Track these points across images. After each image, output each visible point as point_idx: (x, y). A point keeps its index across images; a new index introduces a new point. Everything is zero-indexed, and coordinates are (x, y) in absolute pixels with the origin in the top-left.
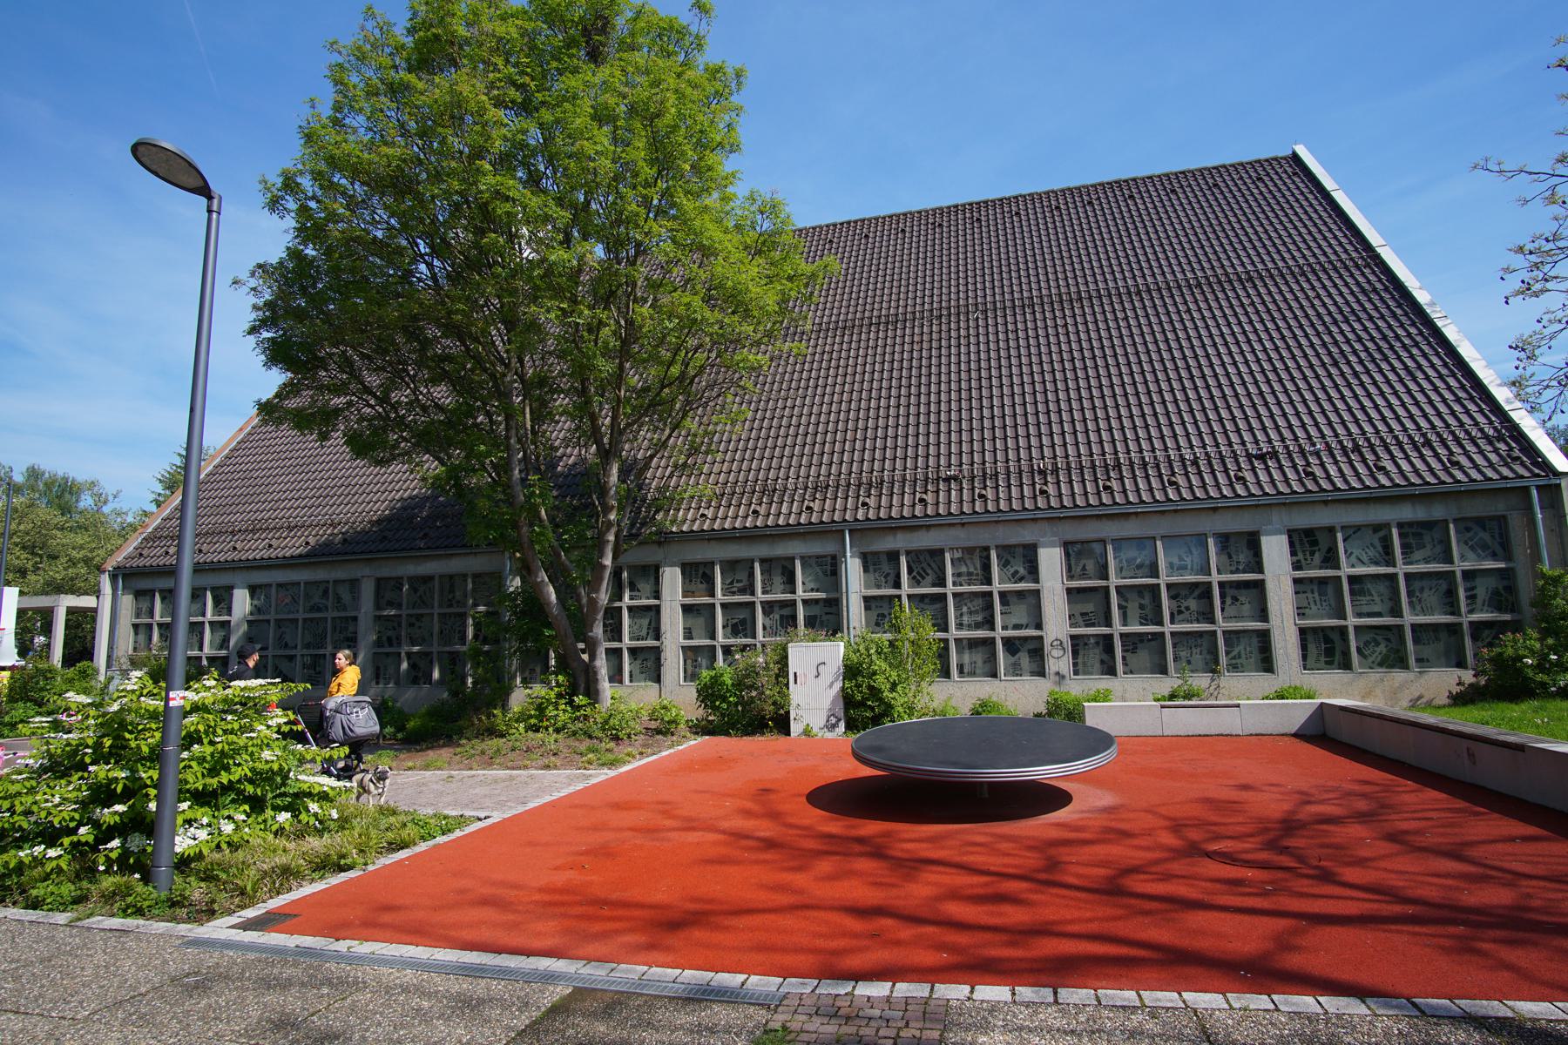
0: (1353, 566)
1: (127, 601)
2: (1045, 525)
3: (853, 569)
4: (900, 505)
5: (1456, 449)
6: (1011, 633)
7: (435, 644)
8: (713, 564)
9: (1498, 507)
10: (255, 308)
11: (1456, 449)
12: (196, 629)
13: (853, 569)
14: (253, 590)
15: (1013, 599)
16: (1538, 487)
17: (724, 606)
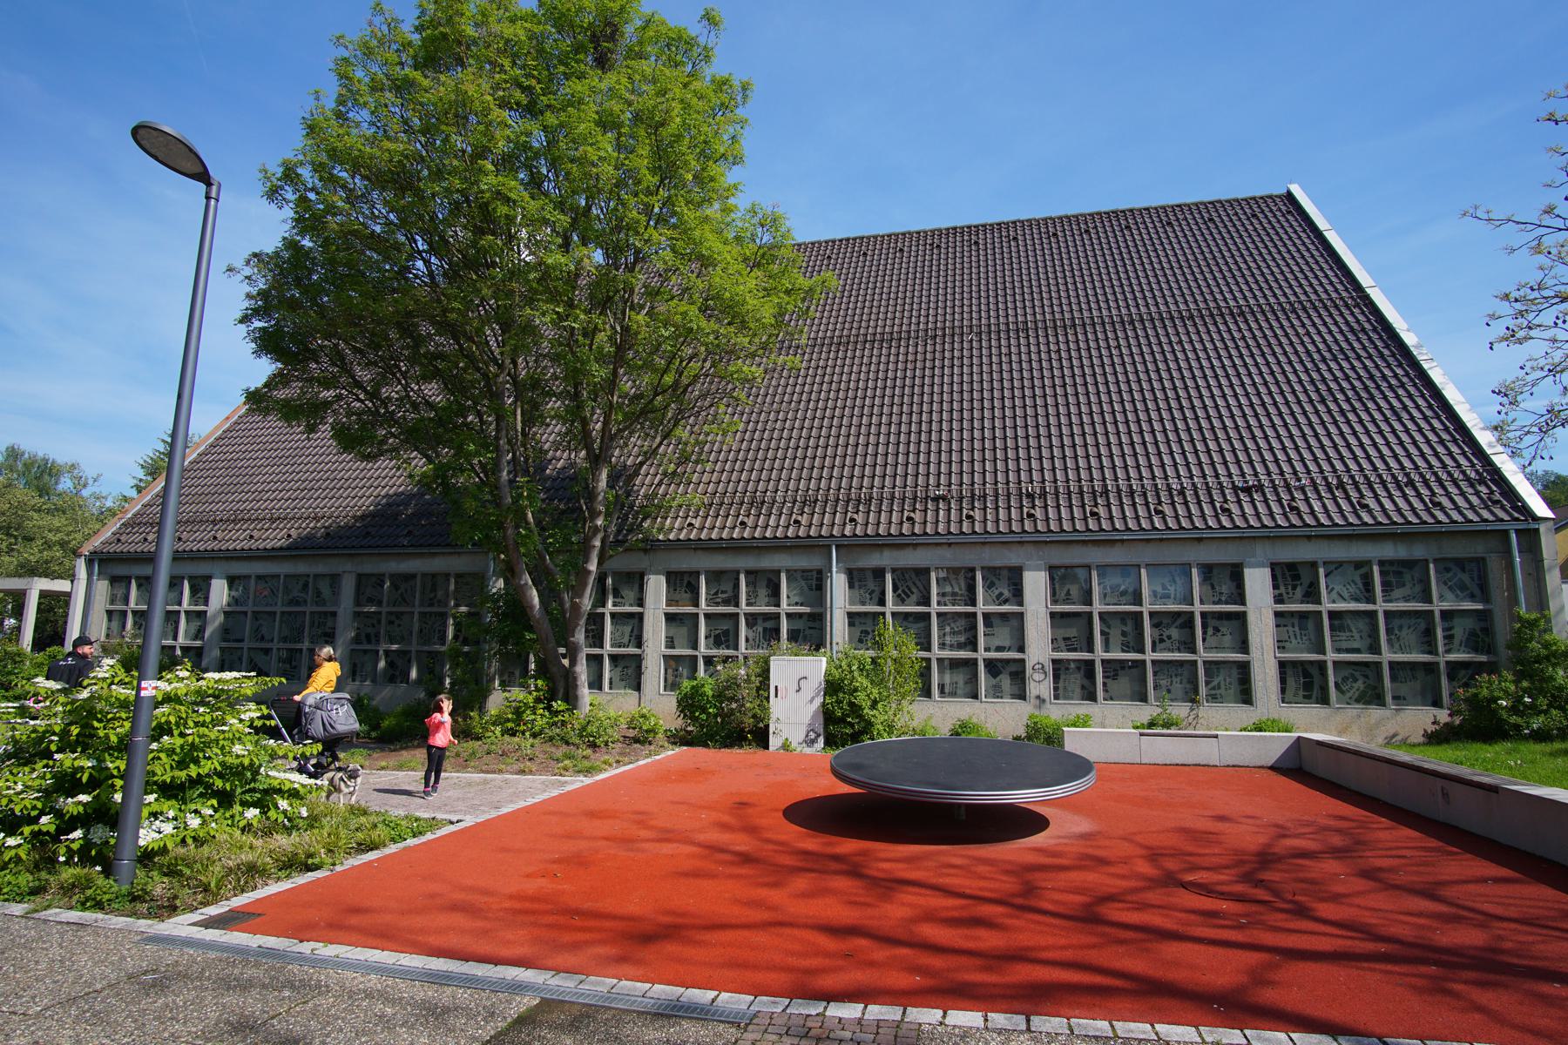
0: (1334, 602)
1: (102, 587)
2: (1030, 549)
3: (838, 584)
4: (888, 523)
5: (1438, 490)
7: (414, 641)
9: (1477, 549)
11: (1438, 490)
12: (171, 618)
13: (838, 584)
14: (232, 581)
17: (707, 616)
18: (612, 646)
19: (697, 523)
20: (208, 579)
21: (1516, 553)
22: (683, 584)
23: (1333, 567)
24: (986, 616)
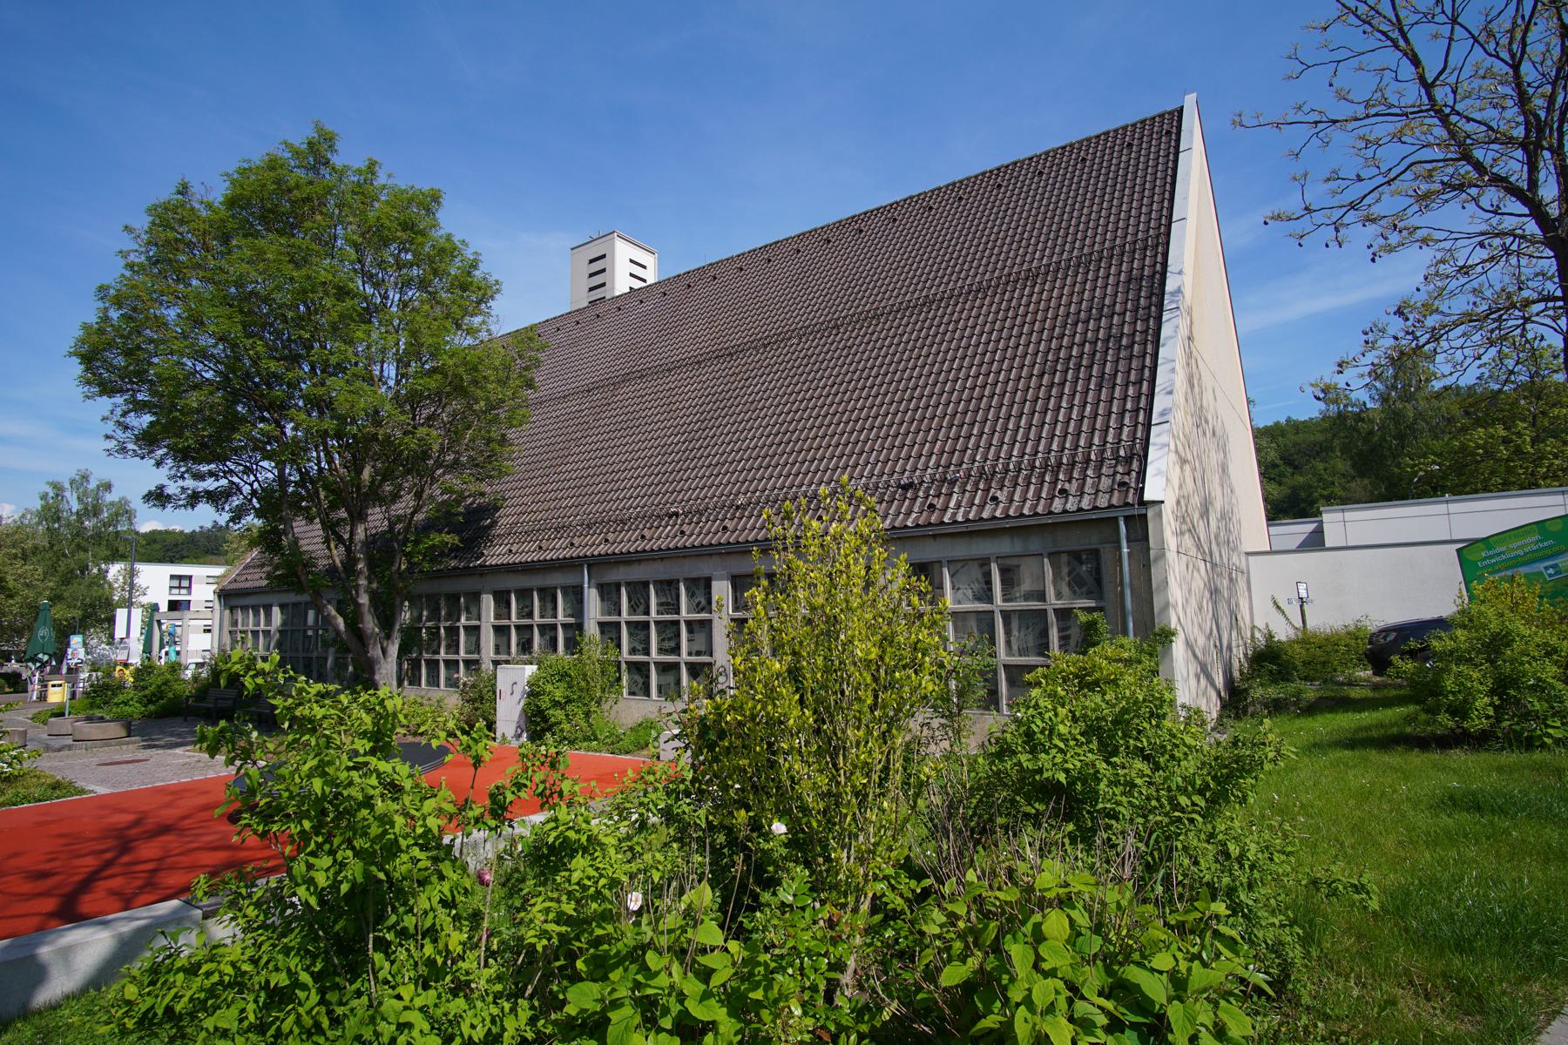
0: (959, 603)
1: (227, 612)
2: (716, 559)
3: (592, 598)
4: (627, 542)
6: (694, 659)
7: (442, 651)
8: (532, 590)
9: (1091, 540)
10: (1327, 393)
12: (639, 629)
13: (592, 598)
14: (282, 607)
15: (696, 628)
16: (1127, 519)
17: (628, 623)
18: (467, 653)
19: (939, 503)
20: (707, 583)
21: (1124, 543)
22: (502, 600)
23: (959, 565)
24: (689, 623)
